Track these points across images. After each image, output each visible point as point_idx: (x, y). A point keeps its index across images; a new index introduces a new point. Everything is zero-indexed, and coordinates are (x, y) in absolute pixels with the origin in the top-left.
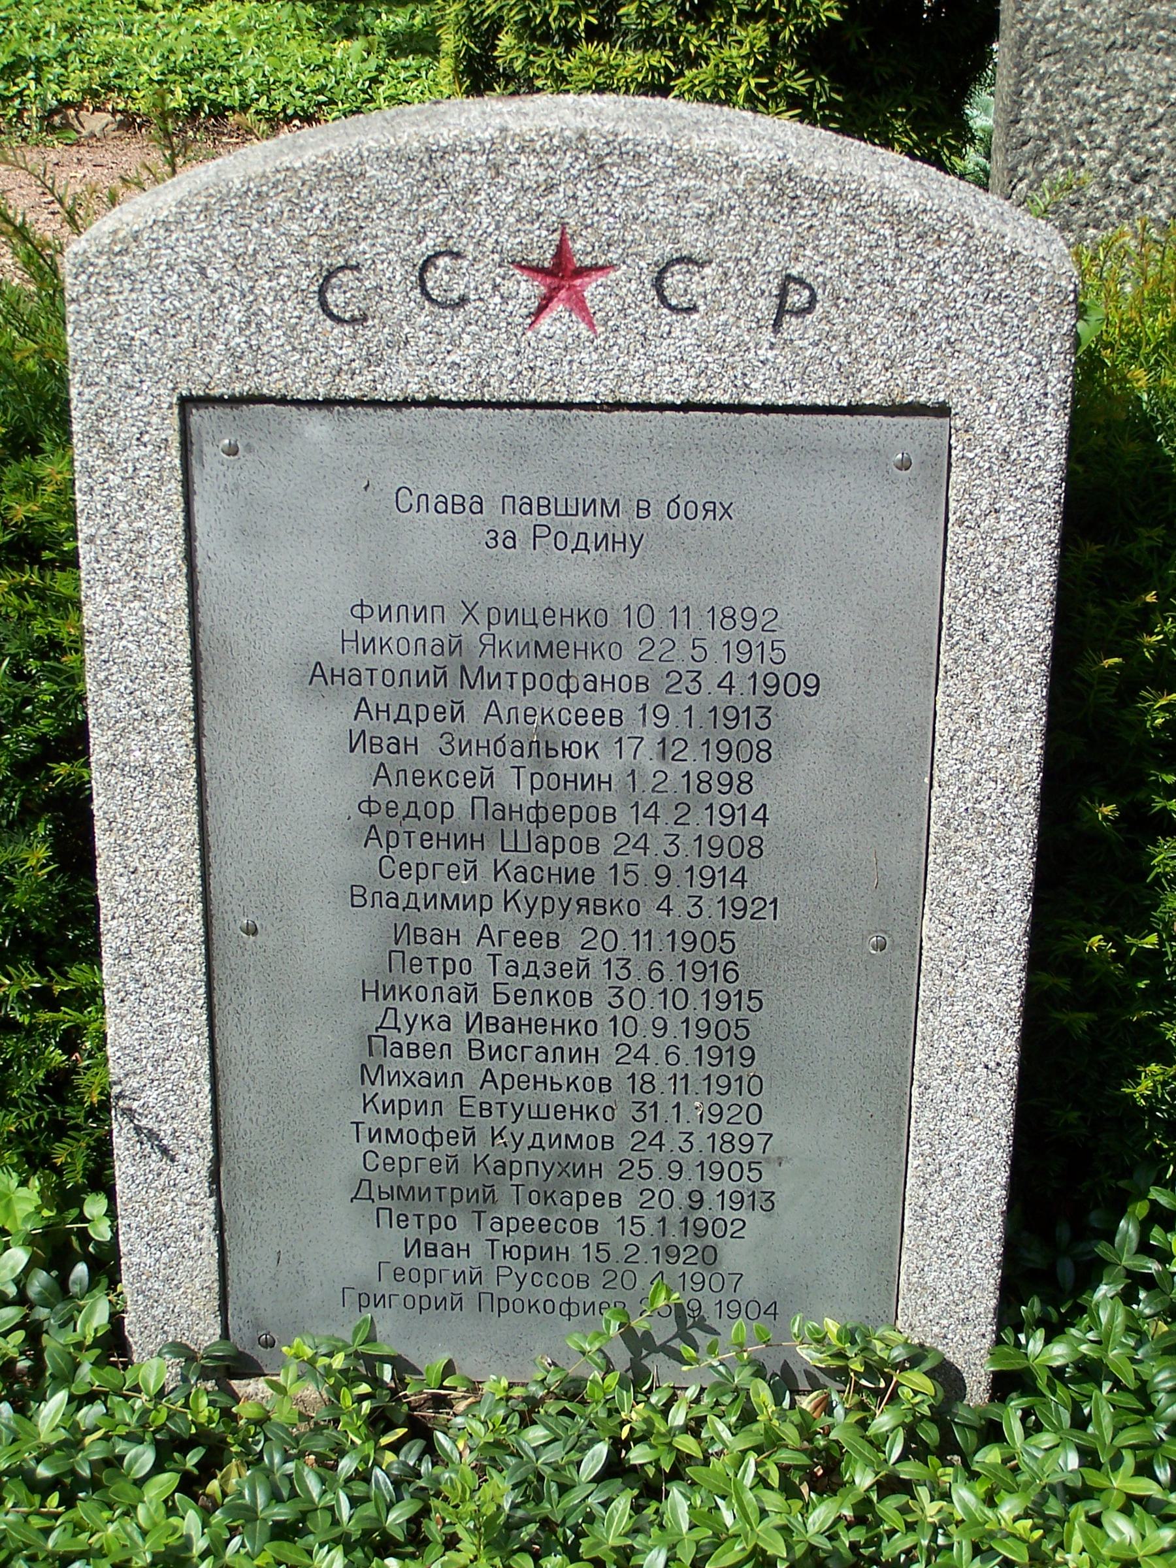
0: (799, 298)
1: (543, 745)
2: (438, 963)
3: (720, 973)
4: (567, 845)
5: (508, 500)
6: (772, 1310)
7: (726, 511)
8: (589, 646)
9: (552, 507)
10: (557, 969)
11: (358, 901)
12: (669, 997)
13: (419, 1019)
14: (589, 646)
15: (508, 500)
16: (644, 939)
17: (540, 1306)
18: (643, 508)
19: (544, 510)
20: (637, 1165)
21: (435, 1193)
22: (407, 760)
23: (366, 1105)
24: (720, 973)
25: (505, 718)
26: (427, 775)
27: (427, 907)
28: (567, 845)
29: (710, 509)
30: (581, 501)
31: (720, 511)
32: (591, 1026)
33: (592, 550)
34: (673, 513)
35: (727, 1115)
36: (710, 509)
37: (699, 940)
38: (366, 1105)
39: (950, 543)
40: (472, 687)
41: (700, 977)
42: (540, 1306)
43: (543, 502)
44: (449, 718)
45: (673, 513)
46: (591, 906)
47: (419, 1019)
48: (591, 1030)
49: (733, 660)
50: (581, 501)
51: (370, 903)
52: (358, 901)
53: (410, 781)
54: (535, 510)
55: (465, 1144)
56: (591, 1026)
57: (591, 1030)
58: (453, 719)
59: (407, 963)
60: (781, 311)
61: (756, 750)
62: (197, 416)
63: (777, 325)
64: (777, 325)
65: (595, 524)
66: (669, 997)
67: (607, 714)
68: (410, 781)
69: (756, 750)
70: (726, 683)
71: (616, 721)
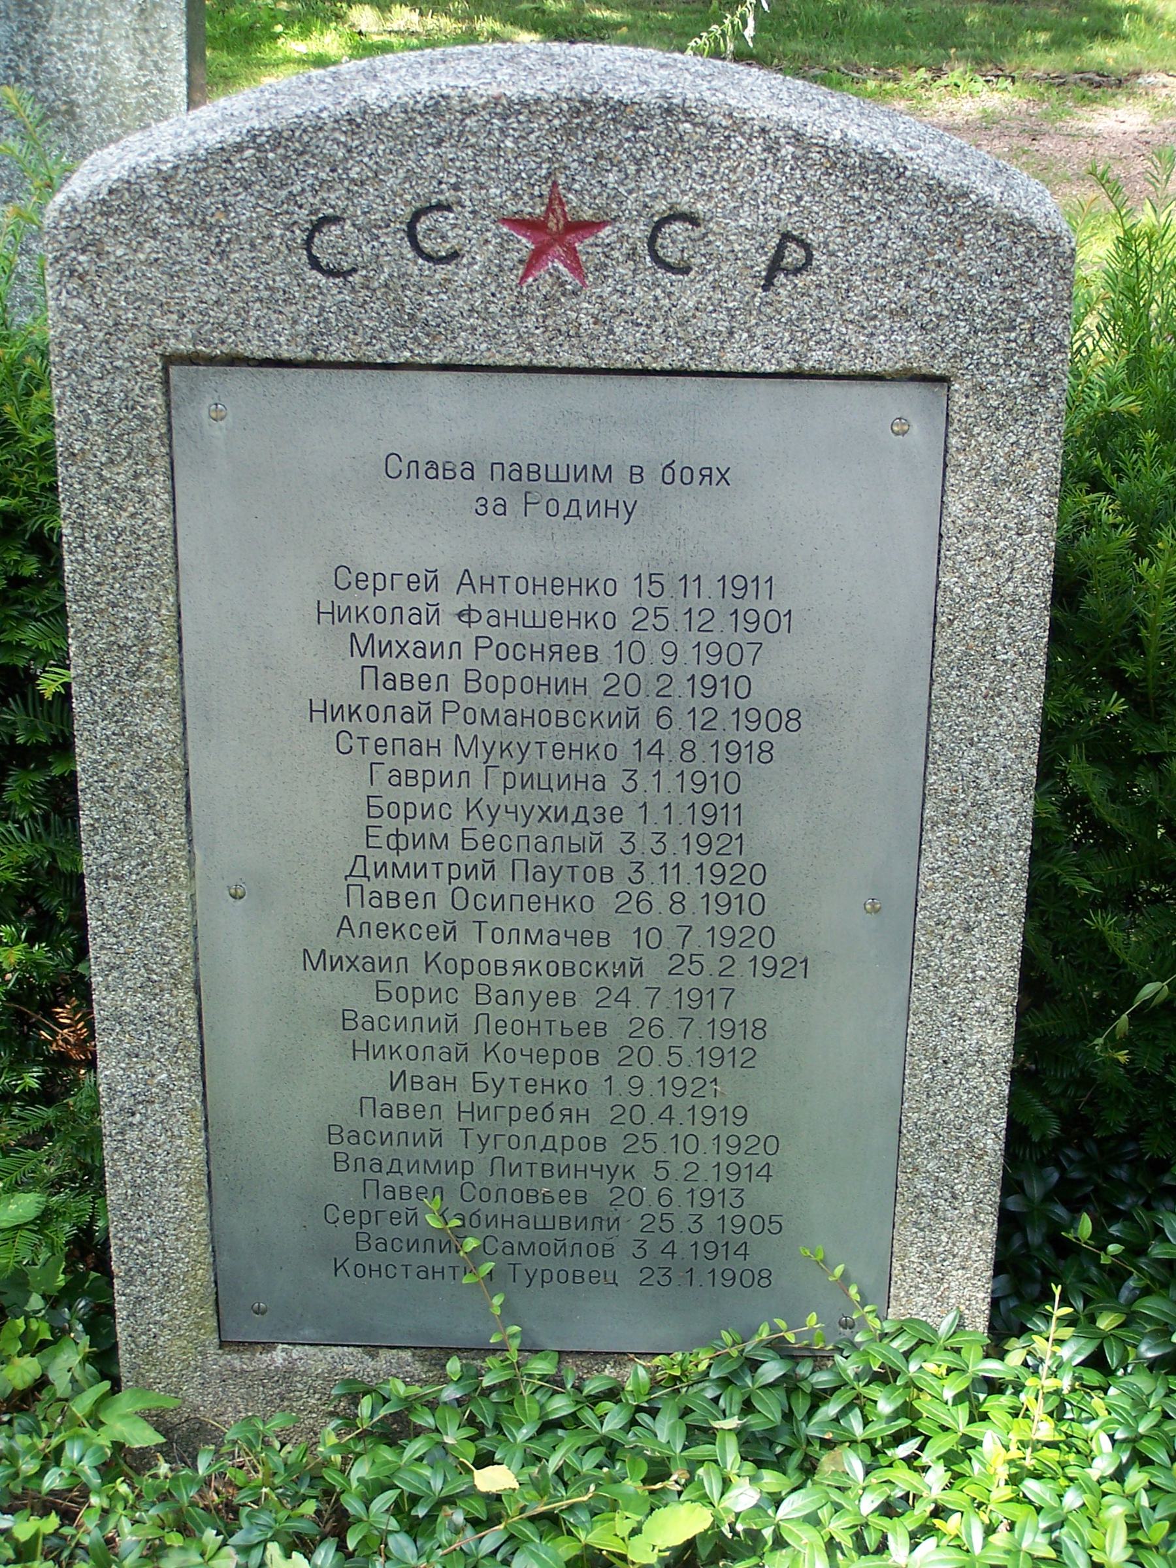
0: (794, 255)
1: (566, 841)
2: (444, 870)
4: (476, 967)
5: (497, 468)
6: (764, 1172)
7: (723, 476)
8: (571, 689)
10: (607, 815)
12: (721, 782)
13: (497, 745)
14: (571, 689)
15: (497, 468)
16: (671, 873)
17: (571, 1086)
18: (636, 473)
19: (534, 476)
20: (651, 613)
21: (431, 870)
22: (396, 979)
25: (357, 931)
27: (377, 875)
28: (476, 967)
29: (706, 474)
30: (507, 906)
31: (716, 476)
32: (581, 1085)
34: (668, 479)
35: (691, 1088)
40: (602, 481)
41: (655, 1022)
42: (571, 1086)
44: (442, 938)
45: (668, 479)
46: (565, 653)
47: (497, 745)
48: (581, 1090)
50: (507, 906)
51: (352, 1168)
53: (373, 931)
54: (524, 478)
56: (581, 1085)
57: (587, 907)
58: (446, 938)
59: (548, 617)
60: (775, 266)
61: (785, 719)
62: (174, 370)
63: (768, 284)
64: (768, 284)
65: (589, 491)
66: (643, 937)
68: (373, 931)
71: (569, 1002)
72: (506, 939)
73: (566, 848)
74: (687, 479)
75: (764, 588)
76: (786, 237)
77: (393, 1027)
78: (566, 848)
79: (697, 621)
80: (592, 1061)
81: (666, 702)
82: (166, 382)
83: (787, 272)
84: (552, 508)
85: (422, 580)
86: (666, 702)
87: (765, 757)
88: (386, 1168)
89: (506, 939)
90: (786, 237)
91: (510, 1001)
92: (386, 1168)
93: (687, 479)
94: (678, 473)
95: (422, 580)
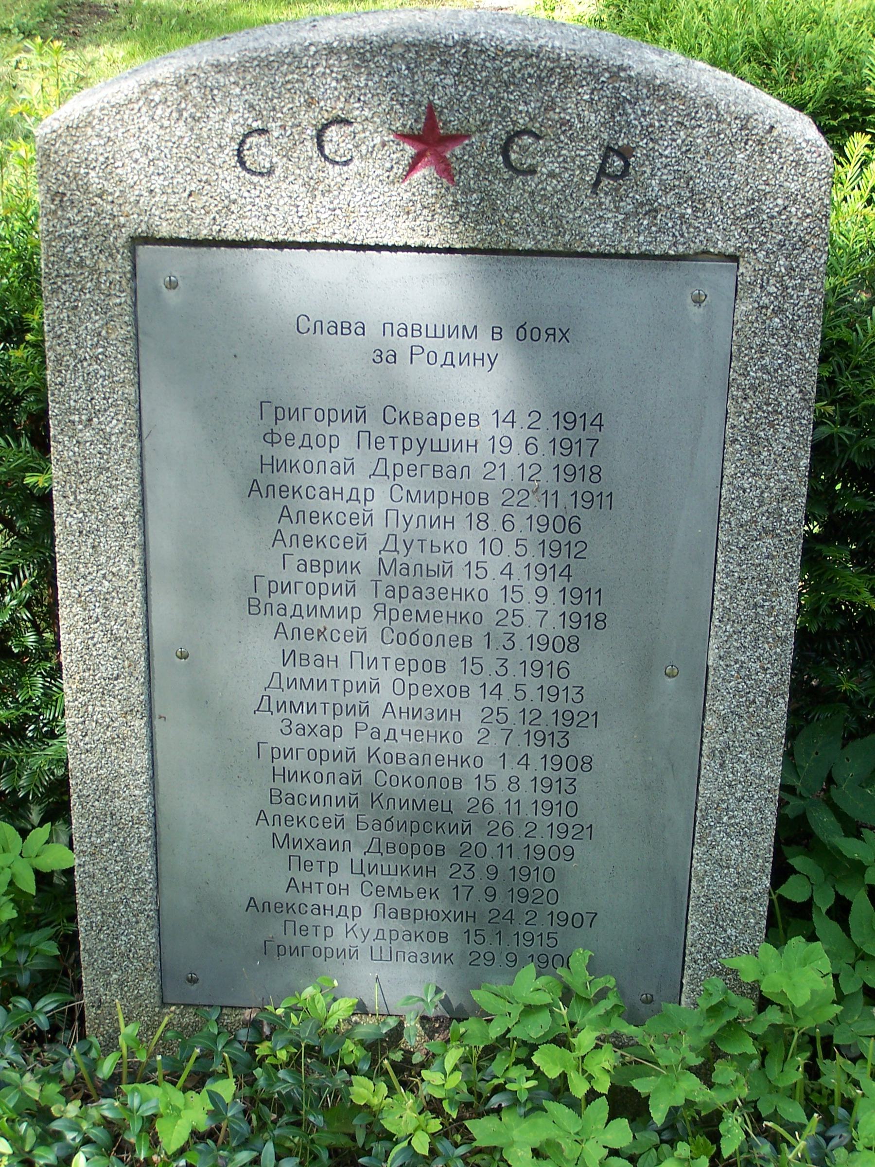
3: (555, 671)
5: (388, 326)
7: (564, 335)
9: (423, 330)
11: (254, 610)
15: (388, 326)
21: (331, 685)
23: (370, 757)
24: (555, 671)
26: (321, 516)
28: (421, 828)
29: (551, 333)
30: (301, 418)
31: (559, 335)
32: (462, 545)
33: (286, 688)
34: (521, 337)
36: (551, 333)
37: (551, 523)
38: (370, 757)
39: (711, 678)
40: (469, 337)
41: (537, 674)
43: (416, 327)
45: (521, 337)
48: (462, 550)
49: (561, 480)
50: (301, 418)
51: (263, 611)
52: (254, 610)
55: (364, 524)
56: (462, 545)
57: (462, 550)
60: (602, 172)
61: (567, 643)
67: (467, 418)
69: (567, 643)
70: (507, 571)
72: (434, 643)
73: (424, 572)
74: (535, 337)
75: (595, 597)
76: (609, 150)
77: (309, 802)
78: (424, 572)
79: (528, 473)
80: (467, 644)
81: (540, 607)
82: (133, 252)
83: (609, 176)
84: (431, 358)
85: (361, 517)
86: (540, 607)
87: (600, 625)
88: (290, 612)
89: (434, 643)
90: (609, 150)
91: (412, 573)
92: (290, 612)
93: (535, 337)
94: (421, 640)
95: (361, 517)
